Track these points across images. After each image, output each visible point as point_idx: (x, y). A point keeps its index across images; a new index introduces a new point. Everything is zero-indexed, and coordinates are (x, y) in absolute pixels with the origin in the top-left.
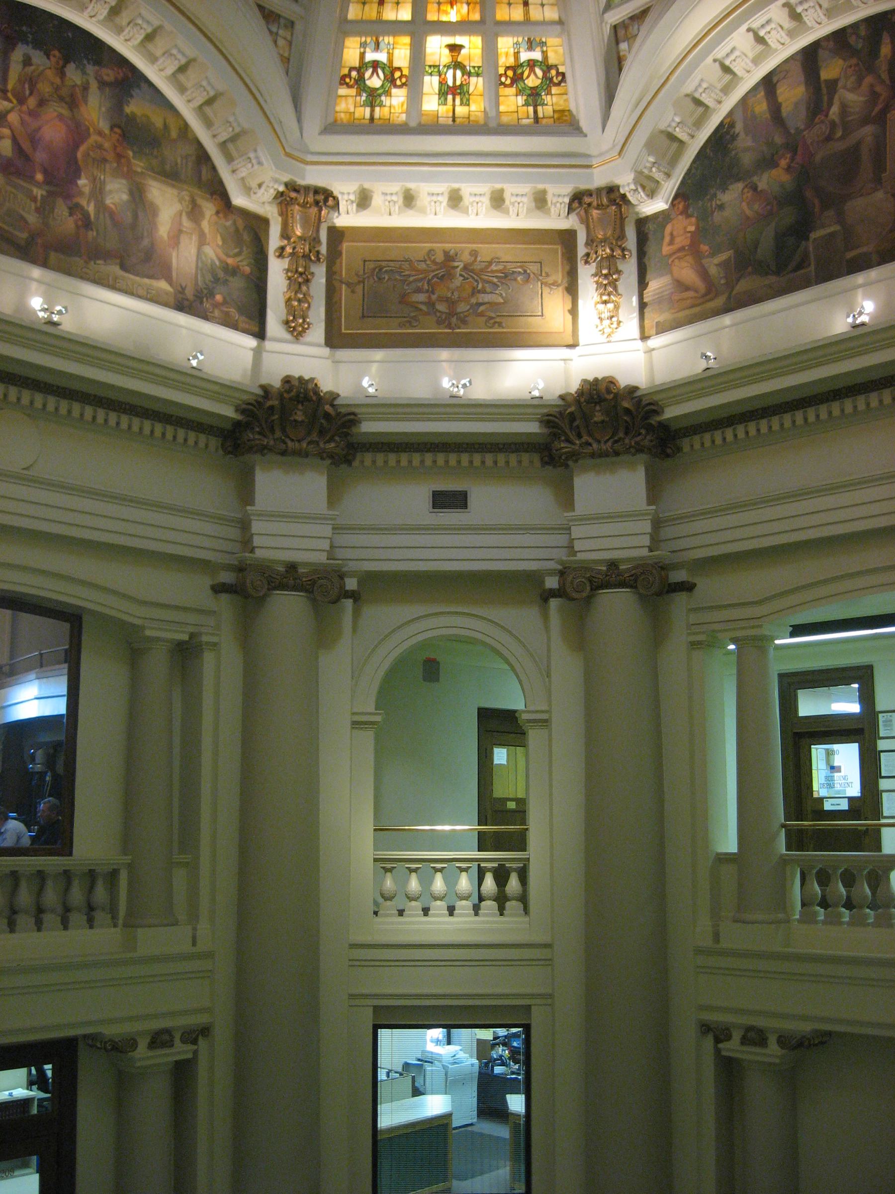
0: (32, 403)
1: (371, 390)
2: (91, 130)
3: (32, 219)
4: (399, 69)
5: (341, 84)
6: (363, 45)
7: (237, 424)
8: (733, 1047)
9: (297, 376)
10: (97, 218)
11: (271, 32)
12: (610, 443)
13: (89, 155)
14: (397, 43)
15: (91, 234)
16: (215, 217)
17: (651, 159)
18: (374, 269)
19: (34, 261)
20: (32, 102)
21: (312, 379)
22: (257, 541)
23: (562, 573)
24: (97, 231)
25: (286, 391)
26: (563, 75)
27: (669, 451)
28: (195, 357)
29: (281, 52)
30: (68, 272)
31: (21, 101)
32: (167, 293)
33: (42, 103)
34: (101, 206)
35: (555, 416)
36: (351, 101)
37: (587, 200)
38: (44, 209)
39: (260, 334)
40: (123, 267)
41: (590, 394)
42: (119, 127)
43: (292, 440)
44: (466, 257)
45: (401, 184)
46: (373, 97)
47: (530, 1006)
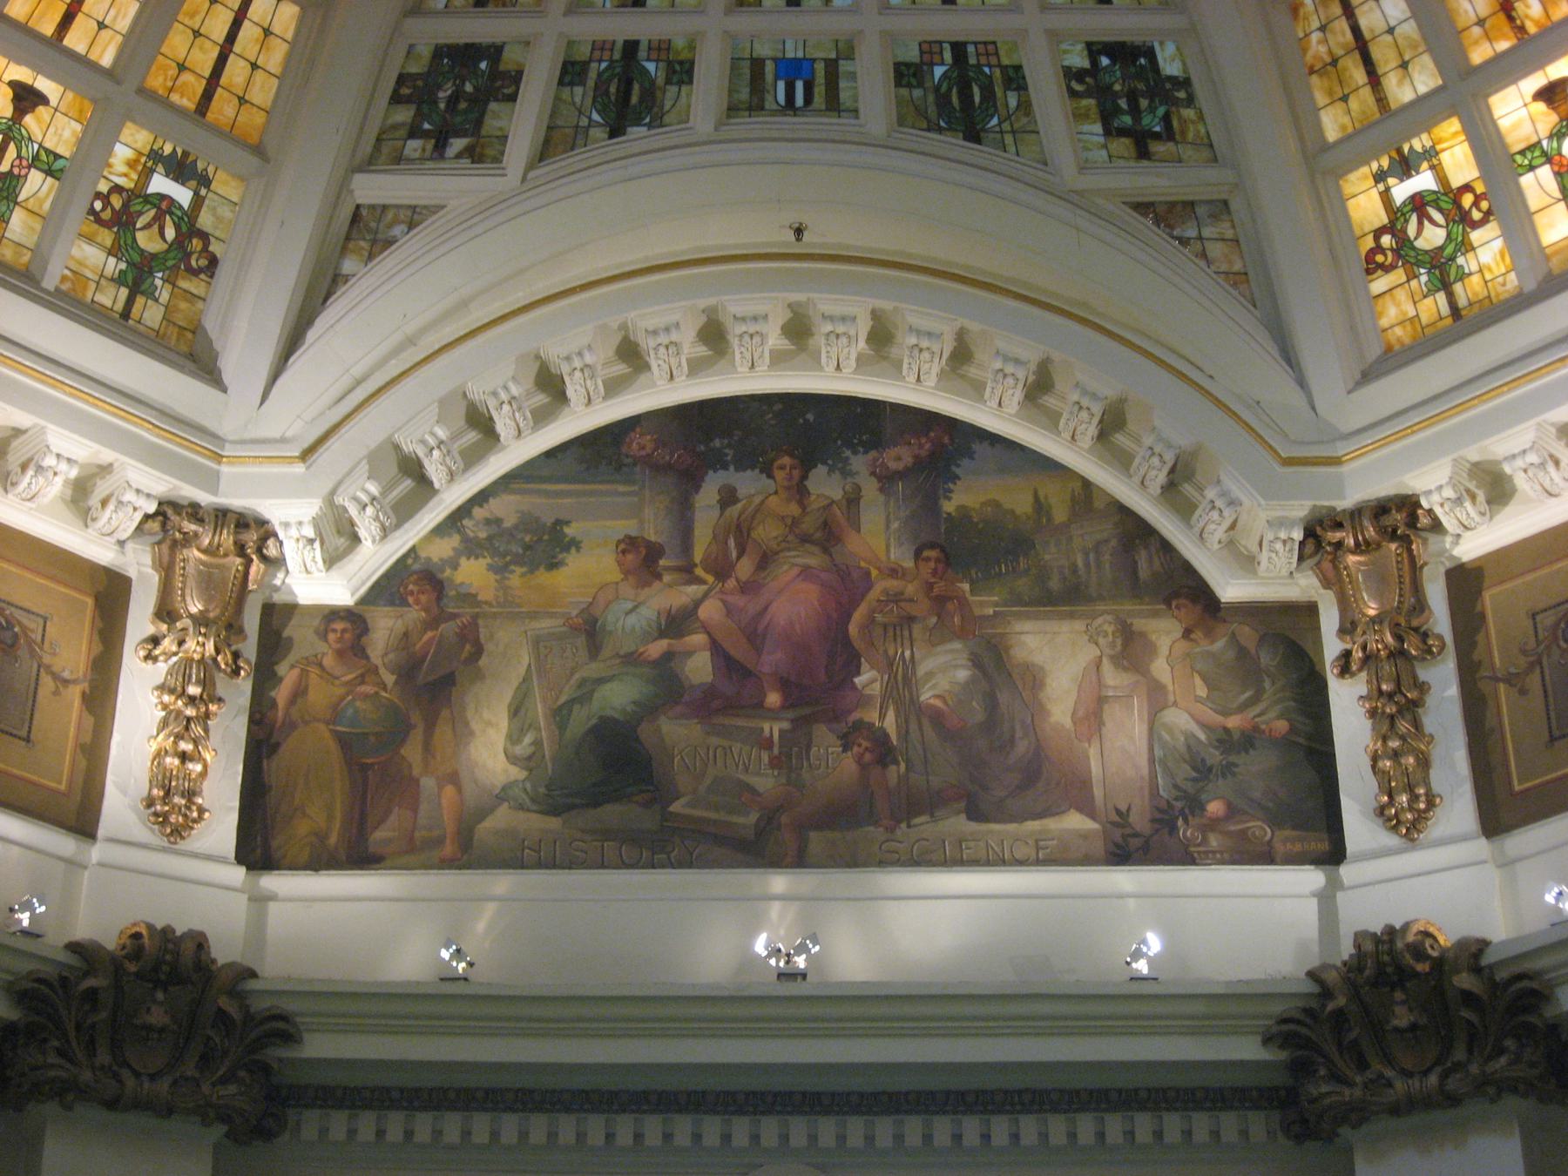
2: (874, 573)
3: (766, 782)
4: (1467, 188)
5: (1369, 272)
6: (1380, 177)
10: (904, 734)
11: (1184, 242)
12: (1433, 1079)
13: (873, 620)
14: (1440, 141)
15: (894, 773)
16: (1183, 646)
17: (373, 488)
18: (1557, 624)
19: (776, 862)
20: (745, 568)
24: (908, 762)
26: (213, 261)
29: (1224, 268)
30: (853, 861)
31: (722, 570)
32: (1085, 836)
33: (765, 561)
34: (910, 709)
35: (1298, 1022)
36: (1401, 294)
38: (789, 756)
39: (1334, 855)
40: (975, 814)
42: (932, 546)
43: (137, 1075)
46: (1441, 269)
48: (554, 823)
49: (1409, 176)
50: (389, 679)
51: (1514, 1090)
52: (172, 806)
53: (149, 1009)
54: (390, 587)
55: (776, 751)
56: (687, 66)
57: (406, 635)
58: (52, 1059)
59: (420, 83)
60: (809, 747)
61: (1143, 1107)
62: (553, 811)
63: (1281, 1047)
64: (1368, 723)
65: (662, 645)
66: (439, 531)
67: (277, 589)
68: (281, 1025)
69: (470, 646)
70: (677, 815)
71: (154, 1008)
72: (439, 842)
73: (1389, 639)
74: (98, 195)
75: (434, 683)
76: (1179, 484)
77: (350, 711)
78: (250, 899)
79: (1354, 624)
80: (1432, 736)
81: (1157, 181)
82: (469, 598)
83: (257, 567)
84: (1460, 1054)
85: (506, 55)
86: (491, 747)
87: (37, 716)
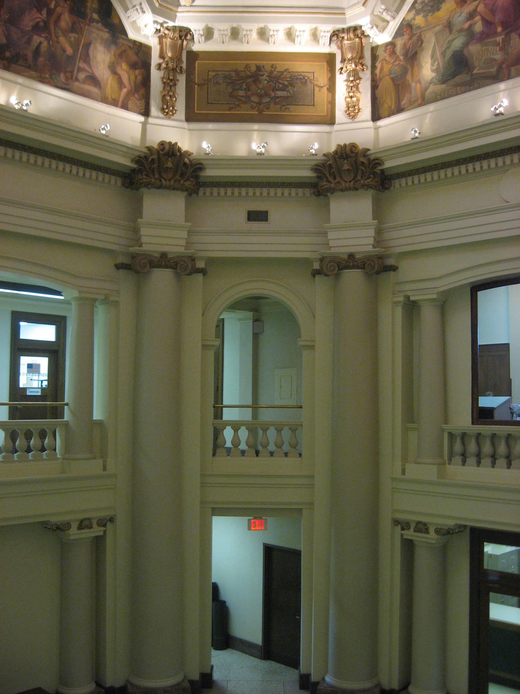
0: (13, 156)
1: (208, 150)
7: (133, 170)
8: (409, 534)
9: (168, 141)
12: (352, 183)
19: (502, 80)
21: (176, 143)
22: (144, 240)
23: (322, 260)
25: (161, 150)
27: (387, 186)
28: (104, 129)
35: (320, 166)
39: (146, 113)
41: (341, 153)
43: (165, 180)
44: (268, 68)
45: (231, 24)
47: (302, 509)
48: (444, 86)
50: (402, 58)
51: (371, 188)
52: (352, 111)
54: (399, 33)
55: (501, 45)
57: (405, 44)
58: (144, 177)
60: (510, 41)
62: (443, 83)
65: (468, 23)
66: (410, 10)
67: (372, 43)
68: (376, 161)
69: (420, 40)
70: (475, 74)
72: (417, 100)
73: (175, 66)
75: (412, 56)
77: (394, 71)
82: (419, 27)
83: (364, 40)
84: (359, 178)
86: (427, 70)
87: (315, 99)
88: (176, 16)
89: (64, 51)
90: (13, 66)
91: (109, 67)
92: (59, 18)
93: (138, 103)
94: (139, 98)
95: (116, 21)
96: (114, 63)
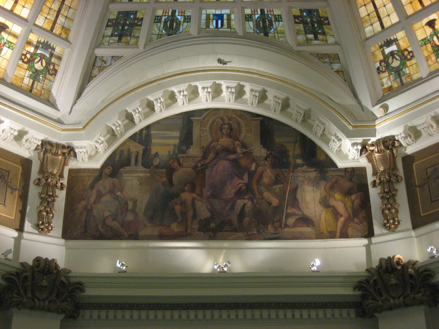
9: (44, 258)
12: (401, 299)
21: (53, 260)
26: (56, 71)
37: (49, 147)
39: (370, 234)
43: (39, 300)
49: (390, 46)
53: (42, 281)
56: (189, 17)
59: (114, 21)
61: (320, 308)
63: (359, 290)
64: (381, 201)
71: (43, 281)
73: (387, 177)
74: (23, 54)
76: (306, 117)
78: (66, 248)
79: (377, 173)
80: (399, 204)
81: (317, 47)
84: (408, 292)
85: (138, 14)
88: (376, 129)
89: (270, 204)
90: (219, 234)
91: (320, 203)
92: (261, 176)
93: (359, 227)
94: (361, 222)
95: (322, 158)
96: (325, 197)
